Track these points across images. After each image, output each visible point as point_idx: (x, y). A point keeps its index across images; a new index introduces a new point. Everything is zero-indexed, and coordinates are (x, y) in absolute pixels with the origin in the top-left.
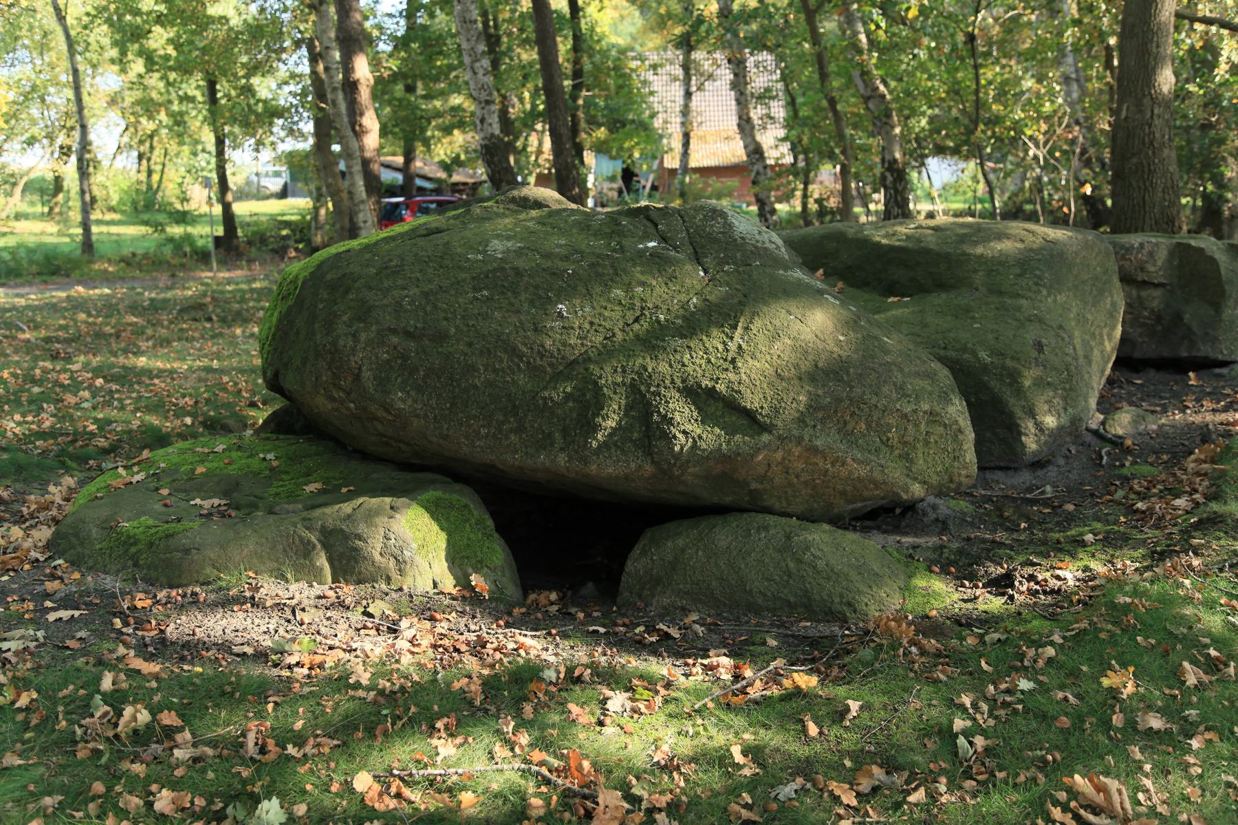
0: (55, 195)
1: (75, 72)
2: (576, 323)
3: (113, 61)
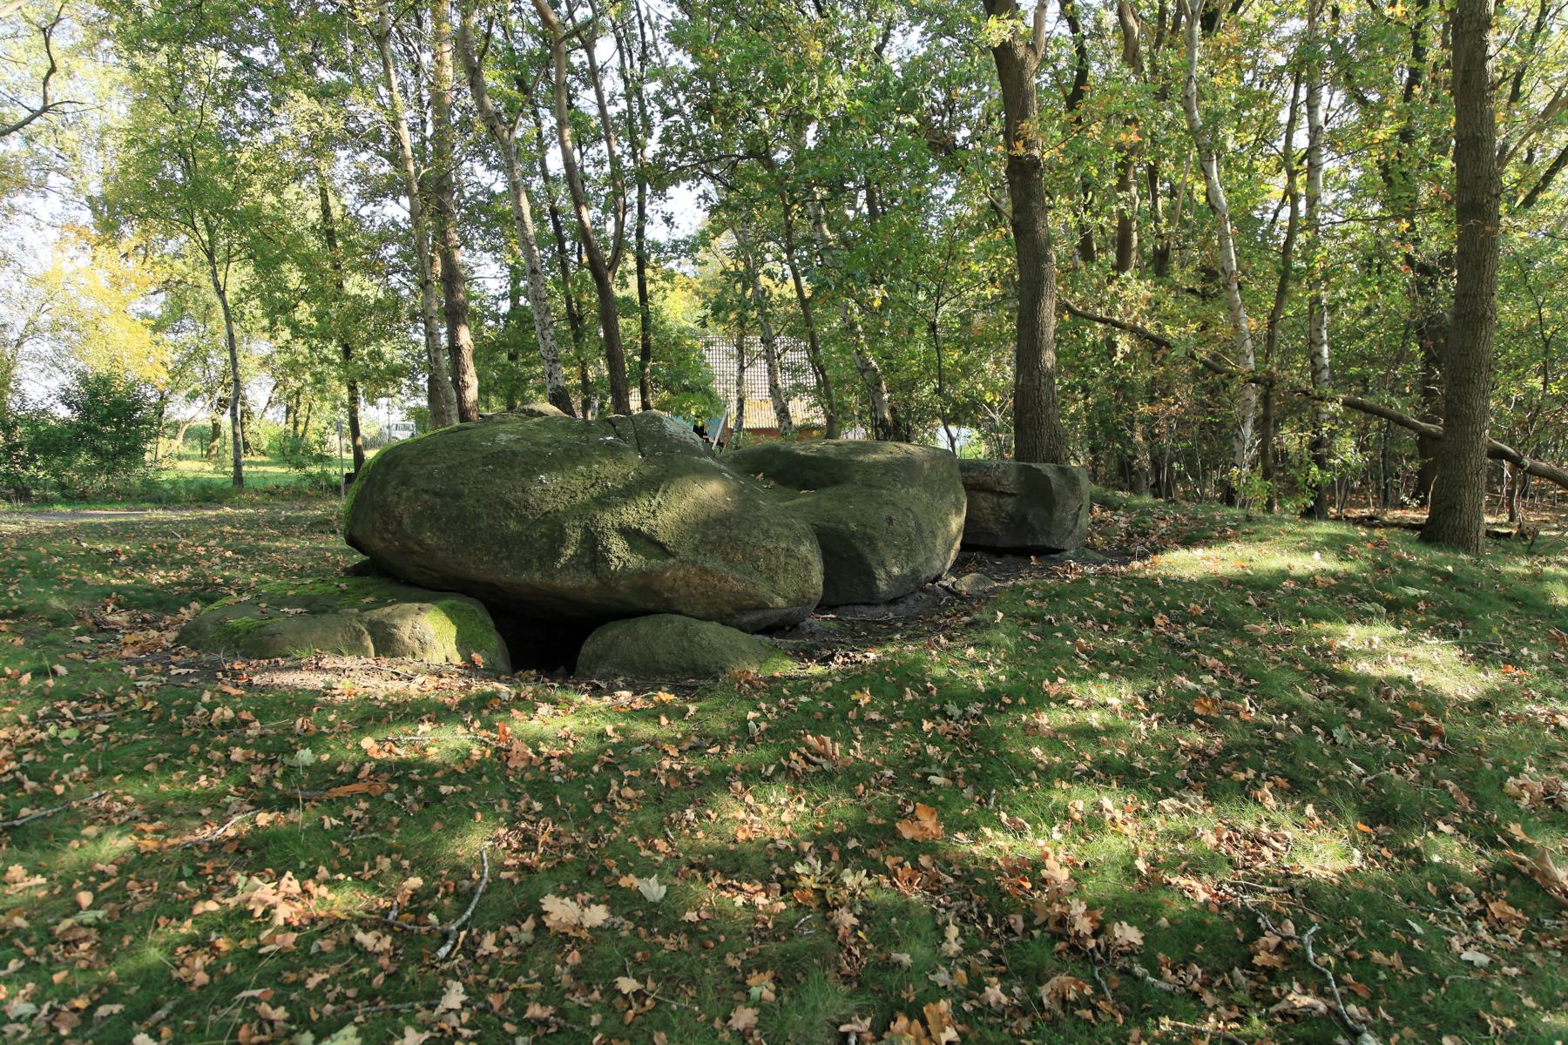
0: (213, 440)
1: (231, 336)
2: (553, 489)
3: (264, 330)
